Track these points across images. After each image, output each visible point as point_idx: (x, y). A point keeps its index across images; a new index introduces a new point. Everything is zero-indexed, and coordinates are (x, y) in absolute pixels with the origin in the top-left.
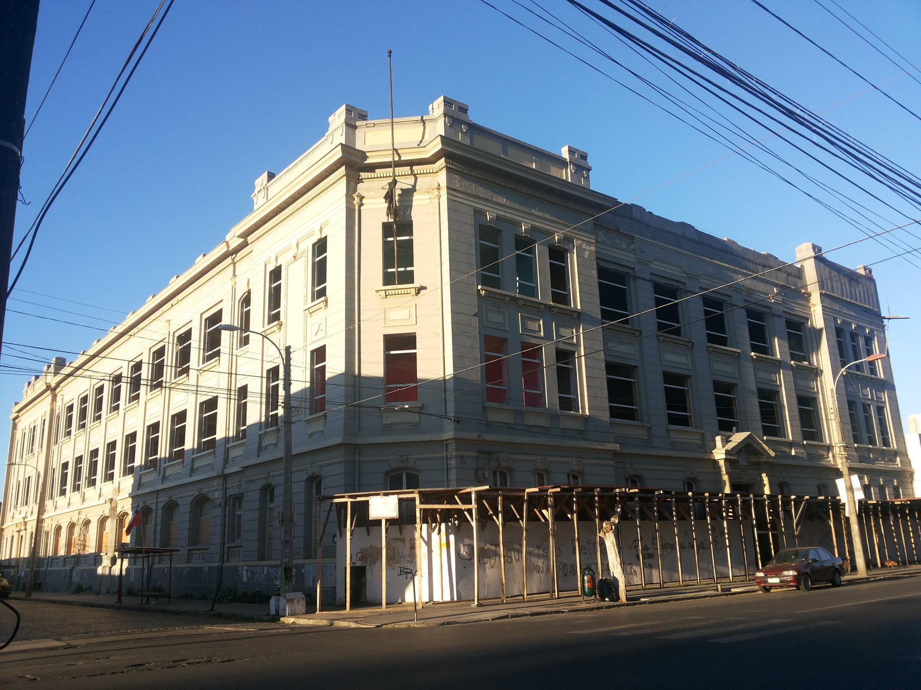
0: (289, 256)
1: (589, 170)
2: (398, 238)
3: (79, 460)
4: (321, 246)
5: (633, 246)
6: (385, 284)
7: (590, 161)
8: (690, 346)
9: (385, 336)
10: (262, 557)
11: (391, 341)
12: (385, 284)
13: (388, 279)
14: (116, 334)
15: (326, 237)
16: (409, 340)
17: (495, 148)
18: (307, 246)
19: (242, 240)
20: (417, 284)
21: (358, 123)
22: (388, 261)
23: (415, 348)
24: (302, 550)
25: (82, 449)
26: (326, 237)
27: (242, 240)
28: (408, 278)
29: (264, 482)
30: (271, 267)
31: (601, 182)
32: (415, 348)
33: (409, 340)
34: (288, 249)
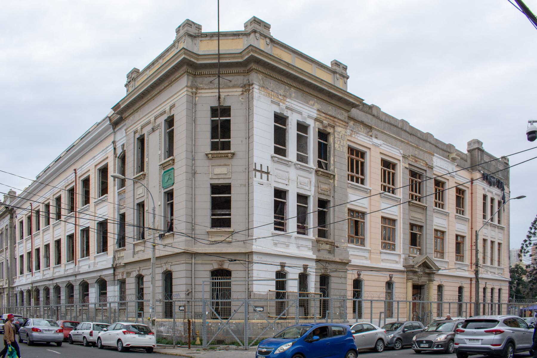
0: (149, 128)
1: (348, 78)
3: (30, 254)
4: (170, 122)
5: (370, 134)
6: (212, 149)
7: (349, 72)
8: (447, 214)
9: (211, 184)
10: (140, 315)
14: (113, 167)
15: (173, 115)
16: (227, 188)
17: (287, 57)
18: (161, 120)
19: (119, 116)
22: (214, 135)
23: (230, 138)
24: (161, 314)
25: (70, 229)
26: (173, 115)
27: (119, 116)
28: (227, 146)
29: (137, 273)
30: (138, 136)
31: (354, 87)
32: (230, 138)
33: (227, 188)
34: (149, 123)
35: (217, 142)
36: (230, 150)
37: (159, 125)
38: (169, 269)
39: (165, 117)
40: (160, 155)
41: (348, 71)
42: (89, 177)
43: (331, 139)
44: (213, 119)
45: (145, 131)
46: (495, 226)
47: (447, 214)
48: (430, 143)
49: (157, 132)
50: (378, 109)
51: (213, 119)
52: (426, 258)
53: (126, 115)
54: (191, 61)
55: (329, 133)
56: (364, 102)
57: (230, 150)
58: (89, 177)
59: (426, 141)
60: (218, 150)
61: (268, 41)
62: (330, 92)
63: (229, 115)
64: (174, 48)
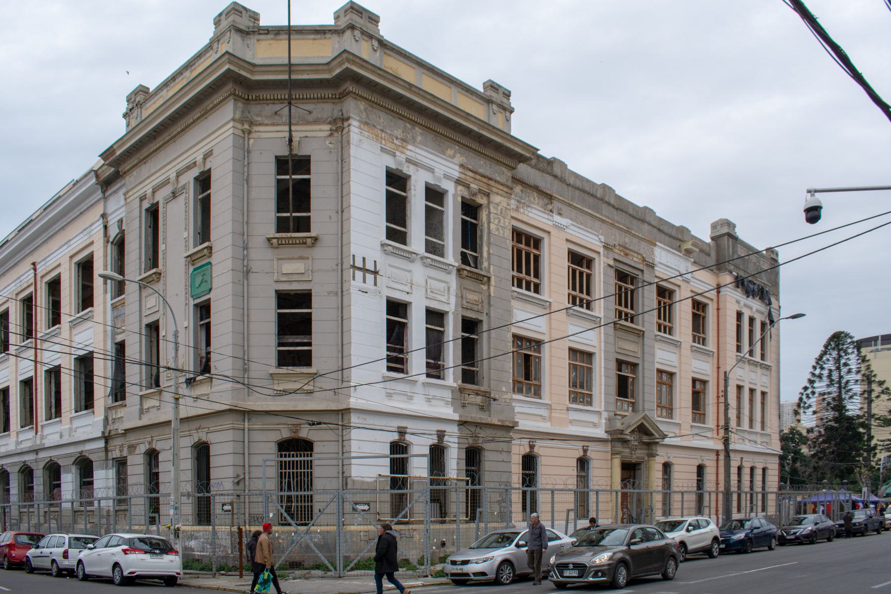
0: (166, 191)
4: (204, 181)
5: (550, 207)
6: (278, 231)
7: (514, 102)
11: (284, 299)
12: (278, 231)
13: (282, 225)
15: (210, 170)
16: (304, 298)
19: (113, 169)
20: (313, 234)
26: (210, 170)
27: (113, 169)
31: (523, 127)
33: (304, 298)
34: (166, 182)
37: (184, 187)
38: (204, 439)
39: (195, 172)
40: (186, 240)
42: (59, 276)
43: (483, 215)
46: (755, 364)
47: (677, 344)
48: (649, 224)
49: (181, 199)
50: (563, 165)
52: (644, 418)
55: (481, 205)
56: (539, 152)
58: (59, 276)
59: (643, 221)
61: (376, 44)
62: (481, 136)
63: (308, 172)
64: (211, 52)
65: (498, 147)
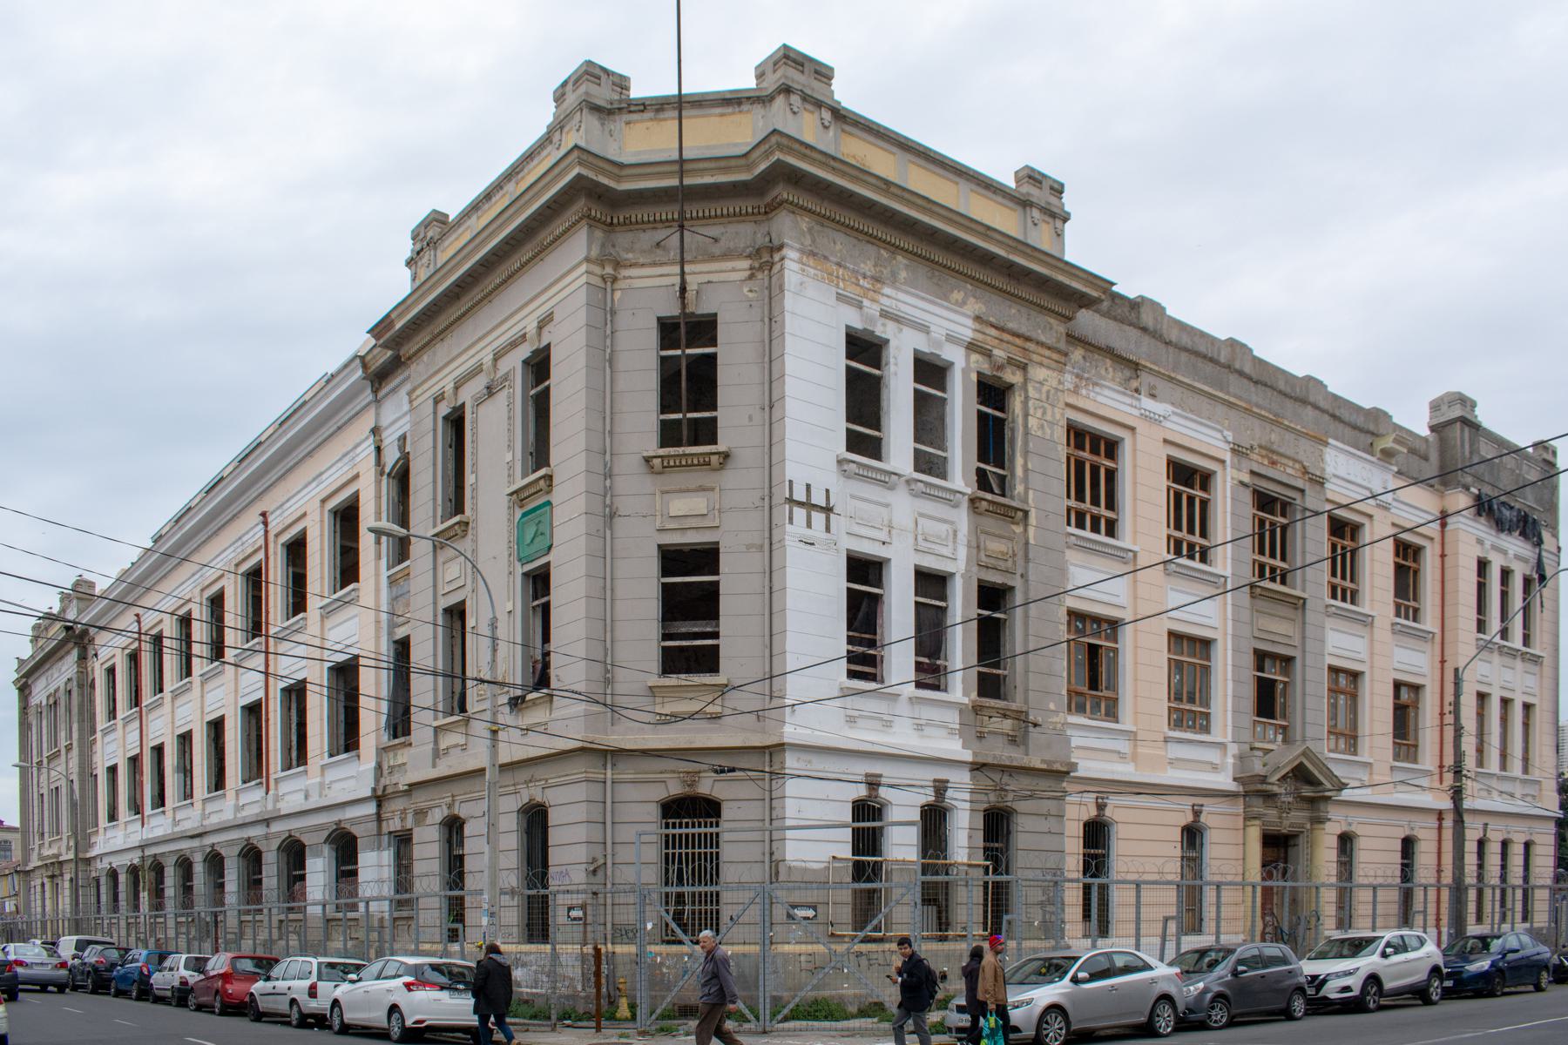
0: (477, 385)
1: (1065, 218)
2: (689, 351)
4: (539, 366)
5: (1135, 384)
7: (1069, 201)
11: (673, 559)
12: (663, 445)
16: (707, 558)
19: (389, 353)
20: (721, 446)
21: (1331, 441)
22: (669, 397)
27: (389, 353)
31: (1086, 246)
33: (707, 558)
34: (477, 371)
35: (679, 421)
36: (716, 443)
37: (506, 378)
38: (539, 799)
39: (524, 351)
41: (1067, 198)
42: (304, 533)
44: (664, 353)
45: (467, 395)
47: (1367, 621)
48: (1316, 407)
49: (501, 398)
50: (1157, 308)
51: (664, 353)
53: (409, 349)
54: (598, 184)
55: (1011, 386)
56: (1114, 288)
57: (716, 443)
58: (304, 533)
59: (1304, 402)
60: (680, 445)
61: (827, 115)
62: (1012, 265)
63: (713, 342)
64: (549, 148)
65: (1042, 283)
